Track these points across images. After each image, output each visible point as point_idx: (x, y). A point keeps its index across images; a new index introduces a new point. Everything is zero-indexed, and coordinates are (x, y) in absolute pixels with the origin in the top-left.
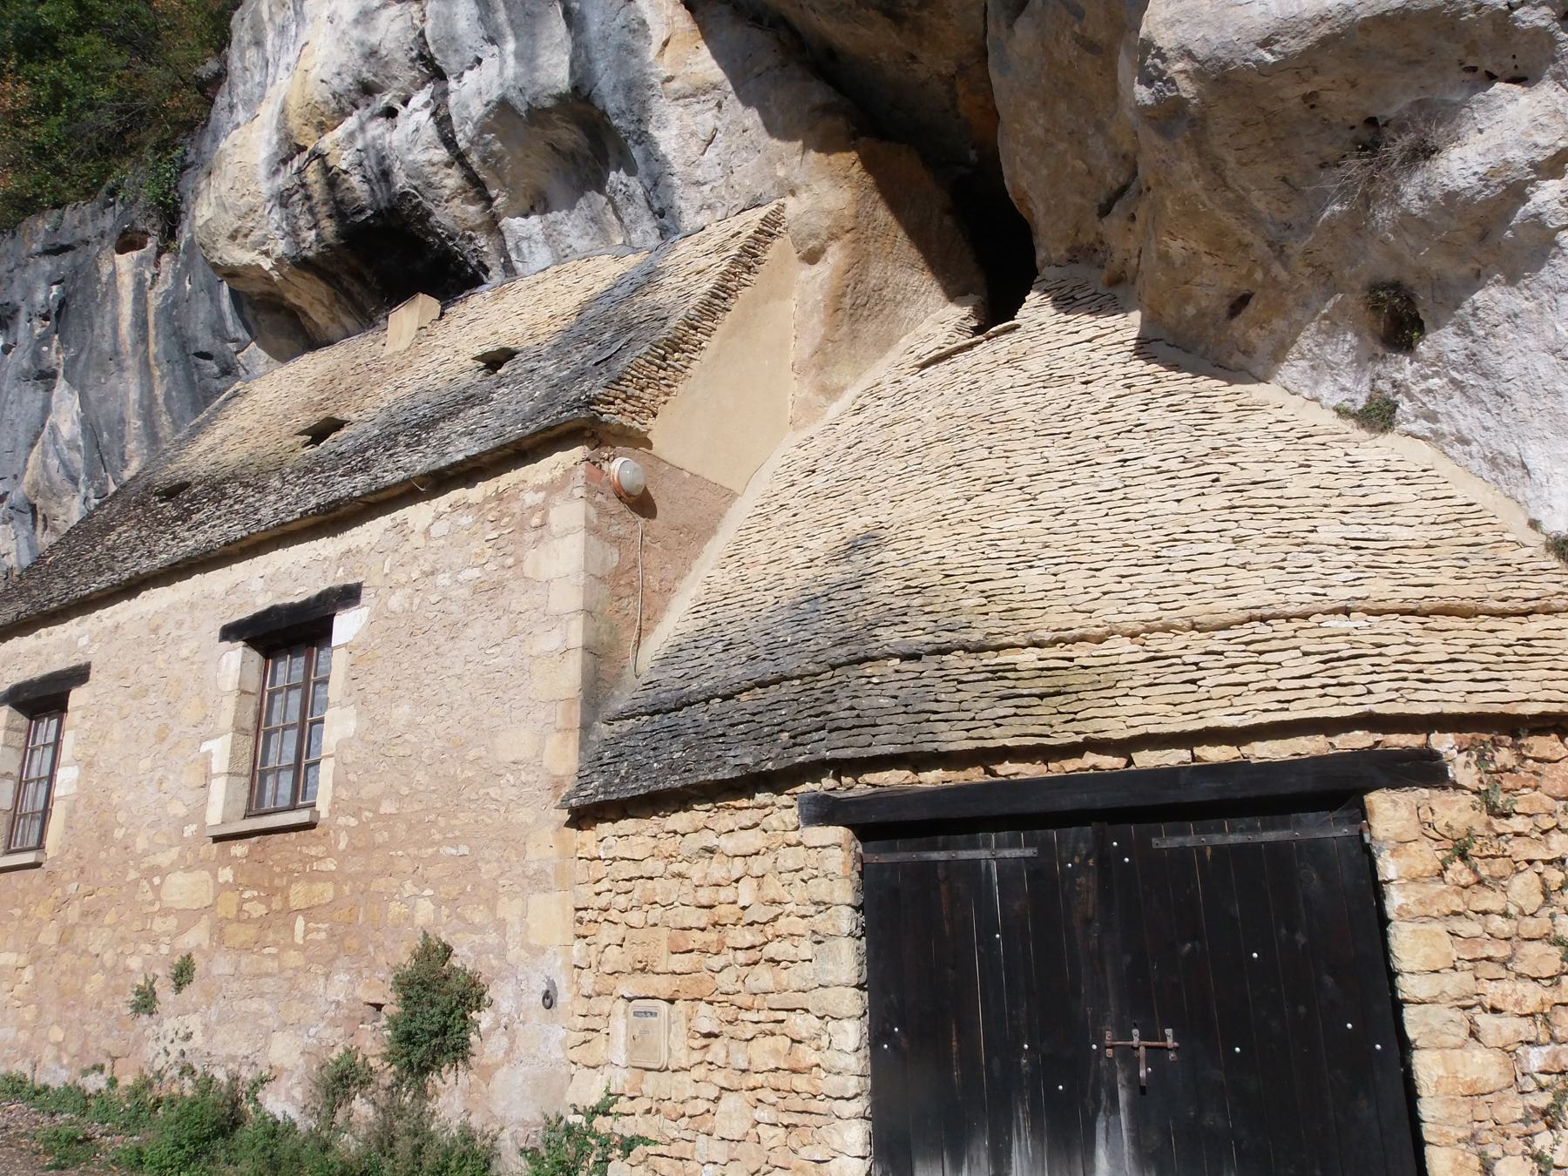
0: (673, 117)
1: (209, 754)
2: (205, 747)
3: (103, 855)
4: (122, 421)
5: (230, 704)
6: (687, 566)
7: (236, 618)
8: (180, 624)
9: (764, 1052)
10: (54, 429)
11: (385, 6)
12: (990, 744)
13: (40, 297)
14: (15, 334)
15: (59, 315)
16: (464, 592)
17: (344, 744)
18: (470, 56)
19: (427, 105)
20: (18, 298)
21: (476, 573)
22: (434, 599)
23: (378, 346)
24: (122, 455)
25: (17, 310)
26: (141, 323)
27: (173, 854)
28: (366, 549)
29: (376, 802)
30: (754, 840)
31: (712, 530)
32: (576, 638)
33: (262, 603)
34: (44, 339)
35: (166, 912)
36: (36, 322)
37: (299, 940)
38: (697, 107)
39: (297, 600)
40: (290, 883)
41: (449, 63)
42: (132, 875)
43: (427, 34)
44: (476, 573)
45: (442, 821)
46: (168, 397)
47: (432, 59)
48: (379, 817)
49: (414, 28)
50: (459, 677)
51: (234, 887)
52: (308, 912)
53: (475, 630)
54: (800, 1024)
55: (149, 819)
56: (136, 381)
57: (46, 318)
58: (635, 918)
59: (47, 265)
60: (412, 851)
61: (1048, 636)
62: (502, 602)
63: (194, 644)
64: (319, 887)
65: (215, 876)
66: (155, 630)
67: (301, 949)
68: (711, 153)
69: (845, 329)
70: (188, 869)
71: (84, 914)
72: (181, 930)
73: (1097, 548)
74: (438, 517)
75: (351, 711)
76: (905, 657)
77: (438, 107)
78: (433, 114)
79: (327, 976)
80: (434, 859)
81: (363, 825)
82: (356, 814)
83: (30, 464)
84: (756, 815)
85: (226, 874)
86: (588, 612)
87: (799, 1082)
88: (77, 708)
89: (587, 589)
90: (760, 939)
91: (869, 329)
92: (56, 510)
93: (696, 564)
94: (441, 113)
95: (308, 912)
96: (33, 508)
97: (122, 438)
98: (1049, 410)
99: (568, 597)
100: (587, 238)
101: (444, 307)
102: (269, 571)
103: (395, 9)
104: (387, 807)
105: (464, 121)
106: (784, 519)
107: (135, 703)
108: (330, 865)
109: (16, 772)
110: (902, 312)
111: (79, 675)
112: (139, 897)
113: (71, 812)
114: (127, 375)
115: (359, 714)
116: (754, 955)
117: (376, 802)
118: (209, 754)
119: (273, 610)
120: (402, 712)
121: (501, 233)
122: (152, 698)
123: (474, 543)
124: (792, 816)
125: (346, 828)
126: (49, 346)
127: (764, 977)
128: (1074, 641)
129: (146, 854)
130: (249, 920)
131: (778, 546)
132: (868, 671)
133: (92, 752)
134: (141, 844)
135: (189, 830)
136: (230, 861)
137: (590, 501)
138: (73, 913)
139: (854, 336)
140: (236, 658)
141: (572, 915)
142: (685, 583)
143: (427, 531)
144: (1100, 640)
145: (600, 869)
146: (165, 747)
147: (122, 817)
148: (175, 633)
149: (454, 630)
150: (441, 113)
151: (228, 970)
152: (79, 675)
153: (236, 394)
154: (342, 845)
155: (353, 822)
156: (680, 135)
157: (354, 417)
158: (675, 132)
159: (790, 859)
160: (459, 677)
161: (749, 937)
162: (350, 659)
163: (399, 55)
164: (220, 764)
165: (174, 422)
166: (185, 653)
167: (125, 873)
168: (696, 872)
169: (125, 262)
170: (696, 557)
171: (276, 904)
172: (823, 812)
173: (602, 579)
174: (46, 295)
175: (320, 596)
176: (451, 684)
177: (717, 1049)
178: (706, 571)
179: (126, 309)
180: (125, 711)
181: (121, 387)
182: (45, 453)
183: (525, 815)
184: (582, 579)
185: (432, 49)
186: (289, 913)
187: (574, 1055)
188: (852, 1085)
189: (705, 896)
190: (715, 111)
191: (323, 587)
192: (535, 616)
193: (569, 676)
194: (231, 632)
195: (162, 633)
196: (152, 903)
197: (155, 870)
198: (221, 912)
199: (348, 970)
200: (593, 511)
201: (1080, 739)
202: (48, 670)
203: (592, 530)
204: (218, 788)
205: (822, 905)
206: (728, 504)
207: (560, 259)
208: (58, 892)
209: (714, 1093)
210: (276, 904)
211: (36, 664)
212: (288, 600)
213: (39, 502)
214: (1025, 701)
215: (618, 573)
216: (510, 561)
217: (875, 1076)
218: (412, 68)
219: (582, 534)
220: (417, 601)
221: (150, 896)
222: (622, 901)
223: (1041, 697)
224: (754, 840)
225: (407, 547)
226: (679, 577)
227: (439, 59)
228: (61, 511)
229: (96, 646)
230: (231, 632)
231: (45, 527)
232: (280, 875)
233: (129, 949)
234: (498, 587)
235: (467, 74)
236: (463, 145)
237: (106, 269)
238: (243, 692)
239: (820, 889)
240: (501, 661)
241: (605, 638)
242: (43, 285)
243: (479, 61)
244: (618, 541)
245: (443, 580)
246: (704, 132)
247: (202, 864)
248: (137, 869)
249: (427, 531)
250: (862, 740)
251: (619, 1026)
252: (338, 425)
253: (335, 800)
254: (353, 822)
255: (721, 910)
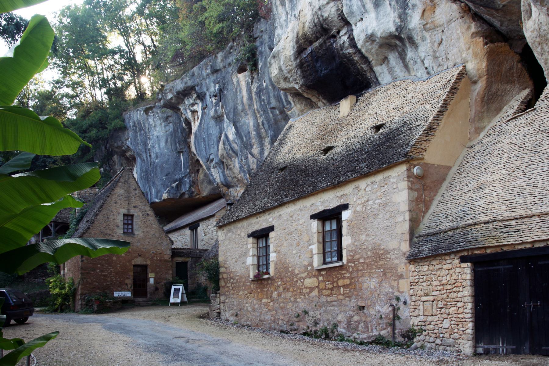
0: (428, 37)
1: (312, 249)
2: (310, 247)
3: (286, 275)
4: (249, 132)
5: (315, 236)
6: (437, 192)
7: (314, 213)
8: (299, 215)
9: (452, 310)
10: (226, 136)
11: (328, 3)
12: (501, 244)
13: (212, 89)
14: (206, 102)
15: (220, 95)
16: (377, 206)
17: (347, 246)
18: (359, 18)
19: (346, 34)
20: (205, 90)
21: (380, 201)
22: (369, 208)
23: (337, 112)
24: (251, 144)
25: (205, 94)
26: (250, 98)
27: (306, 274)
28: (348, 194)
29: (358, 259)
30: (450, 266)
31: (444, 180)
32: (407, 217)
33: (321, 209)
34: (217, 104)
35: (307, 288)
36: (213, 99)
37: (342, 292)
38: (436, 32)
39: (331, 208)
40: (338, 280)
41: (352, 22)
42: (295, 279)
43: (344, 11)
44: (380, 201)
45: (376, 264)
46: (263, 124)
47: (346, 19)
48: (359, 263)
49: (339, 10)
50: (377, 228)
51: (324, 281)
52: (344, 286)
53: (381, 216)
54: (459, 304)
55: (298, 266)
56: (252, 118)
57: (215, 96)
58: (424, 284)
59: (213, 78)
60: (369, 271)
61: (518, 217)
62: (387, 208)
63: (303, 220)
64: (346, 280)
65: (318, 279)
66: (292, 217)
67: (343, 295)
68: (441, 48)
69: (486, 107)
70: (310, 277)
71: (284, 289)
72: (311, 292)
73: (536, 190)
74: (368, 186)
75: (349, 237)
76: (485, 223)
77: (350, 35)
78: (348, 38)
79: (350, 301)
80: (375, 273)
81: (355, 265)
82: (354, 262)
83: (220, 148)
84: (450, 261)
85: (321, 278)
86: (410, 211)
87: (460, 316)
88: (272, 238)
89: (409, 205)
90: (451, 288)
91: (493, 107)
92: (230, 163)
93: (440, 191)
94: (351, 37)
95: (344, 286)
96: (223, 163)
97: (250, 138)
98: (536, 143)
99: (404, 207)
100: (403, 72)
101: (357, 97)
102: (322, 200)
103: (332, 4)
104: (362, 261)
105: (359, 40)
106: (464, 175)
107: (289, 237)
108: (348, 275)
109: (256, 254)
110: (504, 98)
111: (272, 229)
112: (298, 284)
113: (276, 264)
114: (249, 116)
115: (352, 238)
116: (451, 291)
117: (358, 259)
118: (312, 250)
119: (324, 211)
120: (363, 237)
121: (374, 72)
122: (294, 235)
123: (378, 193)
124: (457, 261)
125: (351, 266)
126: (219, 106)
127: (453, 295)
128: (524, 218)
129: (298, 274)
130: (328, 289)
131: (462, 184)
132: (477, 227)
133: (279, 249)
134: (297, 272)
135: (309, 268)
136: (322, 275)
137: (408, 181)
138: (281, 289)
139: (488, 109)
140: (315, 224)
141: (409, 284)
142: (437, 197)
143: (365, 189)
144: (531, 217)
145: (415, 273)
146: (299, 247)
147: (290, 265)
148: (298, 217)
149: (375, 216)
150: (351, 37)
151: (325, 301)
152: (272, 229)
153: (290, 127)
154: (351, 270)
155: (353, 265)
156: (430, 42)
157: (336, 144)
158: (429, 41)
159: (458, 270)
160: (377, 228)
161: (449, 287)
162: (348, 224)
163: (335, 19)
164: (315, 251)
165: (266, 131)
166: (301, 223)
167: (293, 279)
168: (438, 273)
169: (241, 76)
170: (440, 188)
171: (335, 285)
172: (463, 260)
173: (413, 201)
174: (214, 88)
175: (337, 207)
176: (375, 230)
177: (443, 310)
178: (442, 192)
179: (245, 93)
180: (287, 238)
181: (247, 121)
182: (224, 144)
183: (397, 261)
184: (407, 203)
185: (346, 16)
186: (339, 287)
187: (411, 314)
188: (469, 315)
189: (440, 278)
190: (441, 33)
191: (338, 204)
192: (396, 212)
193: (406, 227)
194: (313, 217)
195: (294, 217)
196: (302, 286)
197: (302, 278)
198: (321, 287)
199: (355, 299)
200: (410, 183)
201: (521, 242)
202: (261, 228)
203: (410, 188)
204: (316, 258)
205: (465, 280)
206: (449, 171)
207: (395, 79)
208: (276, 284)
209: (442, 319)
210: (335, 285)
211: (258, 226)
212: (328, 208)
213: (224, 160)
214: (510, 233)
215: (417, 199)
216: (388, 198)
217: (475, 314)
218: (340, 22)
219: (407, 190)
220: (364, 209)
221: (301, 284)
222: (421, 280)
223: (515, 232)
224: (450, 266)
225: (360, 194)
226: (435, 195)
227: (349, 19)
228: (232, 163)
229: (275, 221)
230: (313, 217)
231: (227, 168)
232: (335, 278)
233: (298, 297)
234: (386, 205)
235: (358, 23)
236: (359, 47)
237: (235, 80)
238: (319, 232)
239: (464, 277)
240: (388, 224)
241: (415, 216)
242: (212, 85)
243: (362, 19)
244: (416, 190)
245: (371, 203)
246: (438, 41)
247: (315, 276)
248: (296, 278)
249: (365, 189)
250: (473, 244)
251: (421, 307)
252: (330, 148)
253: (348, 260)
254: (353, 265)
255: (443, 282)
